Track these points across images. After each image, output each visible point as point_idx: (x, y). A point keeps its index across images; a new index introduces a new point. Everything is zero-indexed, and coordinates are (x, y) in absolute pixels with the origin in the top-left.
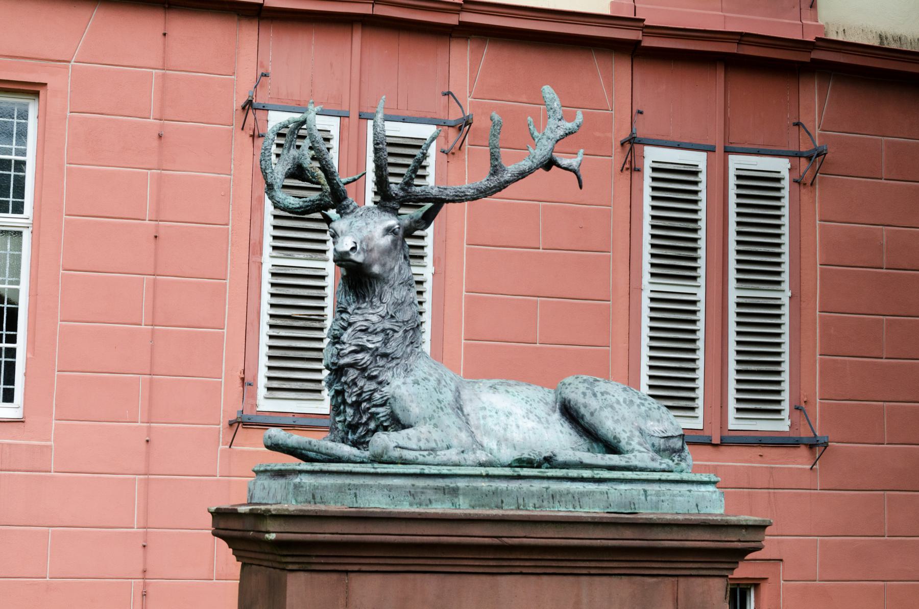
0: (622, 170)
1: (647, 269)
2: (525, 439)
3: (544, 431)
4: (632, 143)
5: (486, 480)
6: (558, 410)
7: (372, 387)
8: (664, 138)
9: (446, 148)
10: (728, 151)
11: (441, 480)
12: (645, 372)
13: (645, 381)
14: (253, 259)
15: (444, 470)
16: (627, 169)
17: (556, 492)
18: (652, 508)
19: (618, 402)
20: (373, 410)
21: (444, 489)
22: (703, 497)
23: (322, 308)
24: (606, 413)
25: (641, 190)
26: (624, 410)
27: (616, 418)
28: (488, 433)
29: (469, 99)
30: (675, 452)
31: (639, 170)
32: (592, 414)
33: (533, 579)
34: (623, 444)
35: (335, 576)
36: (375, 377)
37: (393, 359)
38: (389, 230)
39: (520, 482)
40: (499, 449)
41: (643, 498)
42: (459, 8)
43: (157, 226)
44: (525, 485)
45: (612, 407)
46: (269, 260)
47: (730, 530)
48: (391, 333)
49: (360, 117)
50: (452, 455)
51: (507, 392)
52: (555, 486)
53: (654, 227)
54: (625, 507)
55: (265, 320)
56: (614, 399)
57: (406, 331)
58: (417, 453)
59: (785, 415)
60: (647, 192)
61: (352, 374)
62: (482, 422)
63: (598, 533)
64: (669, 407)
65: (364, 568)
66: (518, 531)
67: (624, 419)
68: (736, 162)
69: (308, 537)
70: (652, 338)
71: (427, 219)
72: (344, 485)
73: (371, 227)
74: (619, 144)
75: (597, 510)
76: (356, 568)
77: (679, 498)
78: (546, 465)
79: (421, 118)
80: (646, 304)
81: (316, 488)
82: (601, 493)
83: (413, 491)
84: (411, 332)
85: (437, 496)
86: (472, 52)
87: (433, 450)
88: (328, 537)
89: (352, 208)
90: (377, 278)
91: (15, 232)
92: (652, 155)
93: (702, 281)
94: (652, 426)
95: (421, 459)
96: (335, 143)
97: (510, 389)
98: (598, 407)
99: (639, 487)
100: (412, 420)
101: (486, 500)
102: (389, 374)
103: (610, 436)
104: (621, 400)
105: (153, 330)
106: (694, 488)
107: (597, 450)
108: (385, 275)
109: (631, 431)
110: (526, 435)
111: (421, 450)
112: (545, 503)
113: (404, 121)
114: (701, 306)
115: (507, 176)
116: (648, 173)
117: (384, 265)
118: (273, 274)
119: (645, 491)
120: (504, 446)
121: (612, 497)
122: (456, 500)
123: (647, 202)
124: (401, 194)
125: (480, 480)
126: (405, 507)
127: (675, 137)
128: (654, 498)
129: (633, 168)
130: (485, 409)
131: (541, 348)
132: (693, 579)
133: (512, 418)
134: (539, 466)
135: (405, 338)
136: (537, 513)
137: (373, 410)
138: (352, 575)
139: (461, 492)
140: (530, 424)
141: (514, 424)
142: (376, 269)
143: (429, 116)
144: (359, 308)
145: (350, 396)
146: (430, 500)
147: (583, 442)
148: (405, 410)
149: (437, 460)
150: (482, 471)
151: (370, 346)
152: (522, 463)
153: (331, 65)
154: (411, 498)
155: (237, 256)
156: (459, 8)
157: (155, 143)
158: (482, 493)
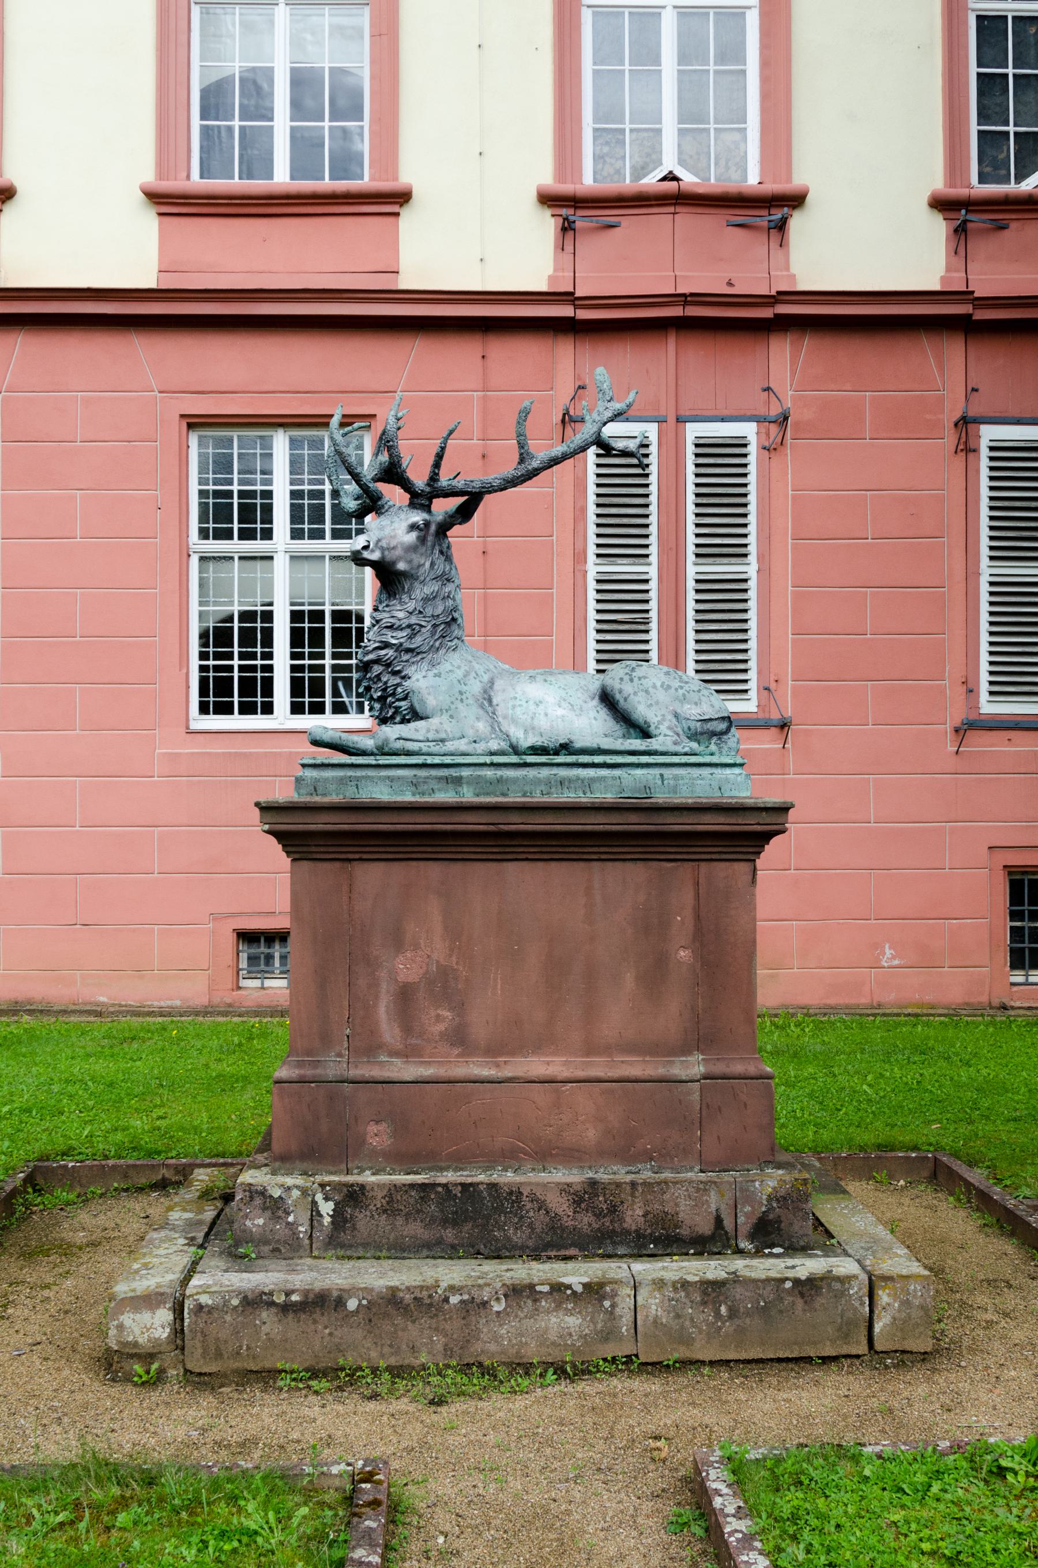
0: (956, 452)
1: (985, 552)
2: (552, 727)
3: (575, 718)
4: (966, 423)
5: (492, 768)
6: (597, 698)
7: (395, 682)
8: (1003, 415)
9: (767, 444)
10: (681, 420)
11: (446, 770)
12: (691, 656)
13: (691, 666)
14: (578, 567)
15: (448, 760)
16: (962, 450)
17: (564, 779)
18: (669, 793)
19: (654, 686)
20: (397, 704)
21: (447, 778)
22: (727, 780)
23: (647, 611)
24: (641, 697)
25: (978, 471)
26: (661, 695)
27: (649, 702)
28: (514, 721)
29: (790, 393)
30: (716, 735)
31: (974, 451)
32: (626, 699)
33: (540, 864)
34: (652, 729)
35: (338, 864)
36: (399, 672)
37: (418, 653)
38: (413, 527)
39: (528, 769)
40: (526, 738)
41: (660, 782)
42: (772, 300)
43: (485, 542)
44: (531, 773)
45: (647, 692)
46: (593, 568)
47: (747, 813)
48: (418, 627)
49: (678, 421)
50: (462, 745)
51: (546, 681)
52: (563, 772)
53: (991, 508)
54: (639, 792)
55: (592, 625)
56: (650, 684)
57: (435, 626)
58: (421, 744)
59: (753, 694)
60: (984, 473)
61: (377, 669)
62: (510, 712)
63: (601, 818)
64: (718, 691)
65: (365, 856)
66: (515, 818)
67: (657, 703)
68: (694, 431)
69: (301, 827)
70: (991, 623)
71: (465, 513)
72: (345, 777)
73: (396, 525)
74: (952, 425)
75: (609, 795)
76: (357, 856)
77: (699, 782)
78: (564, 752)
79: (741, 416)
80: (984, 588)
81: (317, 780)
82: (614, 778)
83: (414, 781)
84: (442, 626)
85: (440, 786)
86: (792, 344)
87: (443, 741)
88: (320, 827)
89: (386, 507)
90: (404, 574)
91: (263, 558)
92: (989, 434)
93: (654, 559)
94: (690, 709)
95: (425, 749)
96: (653, 449)
97: (549, 678)
98: (632, 692)
99: (656, 771)
100: (429, 712)
101: (491, 788)
102: (414, 668)
103: (641, 721)
104: (659, 684)
105: (486, 641)
106: (718, 771)
107: (634, 735)
108: (413, 572)
109: (663, 715)
110: (554, 723)
111: (428, 741)
112: (553, 790)
113: (723, 420)
114: (653, 585)
115: (535, 464)
116: (984, 453)
117: (410, 562)
118: (598, 581)
119: (662, 775)
120: (530, 734)
121: (625, 782)
122: (460, 789)
123: (984, 483)
124: (428, 489)
125: (485, 768)
126: (408, 797)
127: (1014, 412)
128: (672, 782)
129: (968, 449)
130: (516, 698)
131: (873, 639)
132: (505, 864)
133: (541, 707)
134: (556, 753)
135: (433, 634)
136: (546, 799)
137: (397, 704)
138: (355, 863)
139: (464, 781)
140: (560, 712)
141: (542, 713)
142: (401, 566)
143: (749, 413)
144: (387, 606)
145: (375, 692)
146: (433, 790)
147: (617, 729)
148: (422, 701)
149: (442, 751)
150: (488, 760)
151: (394, 641)
152: (536, 750)
153: (647, 372)
154: (413, 789)
155: (562, 566)
156: (772, 300)
157: (480, 462)
158: (486, 782)
